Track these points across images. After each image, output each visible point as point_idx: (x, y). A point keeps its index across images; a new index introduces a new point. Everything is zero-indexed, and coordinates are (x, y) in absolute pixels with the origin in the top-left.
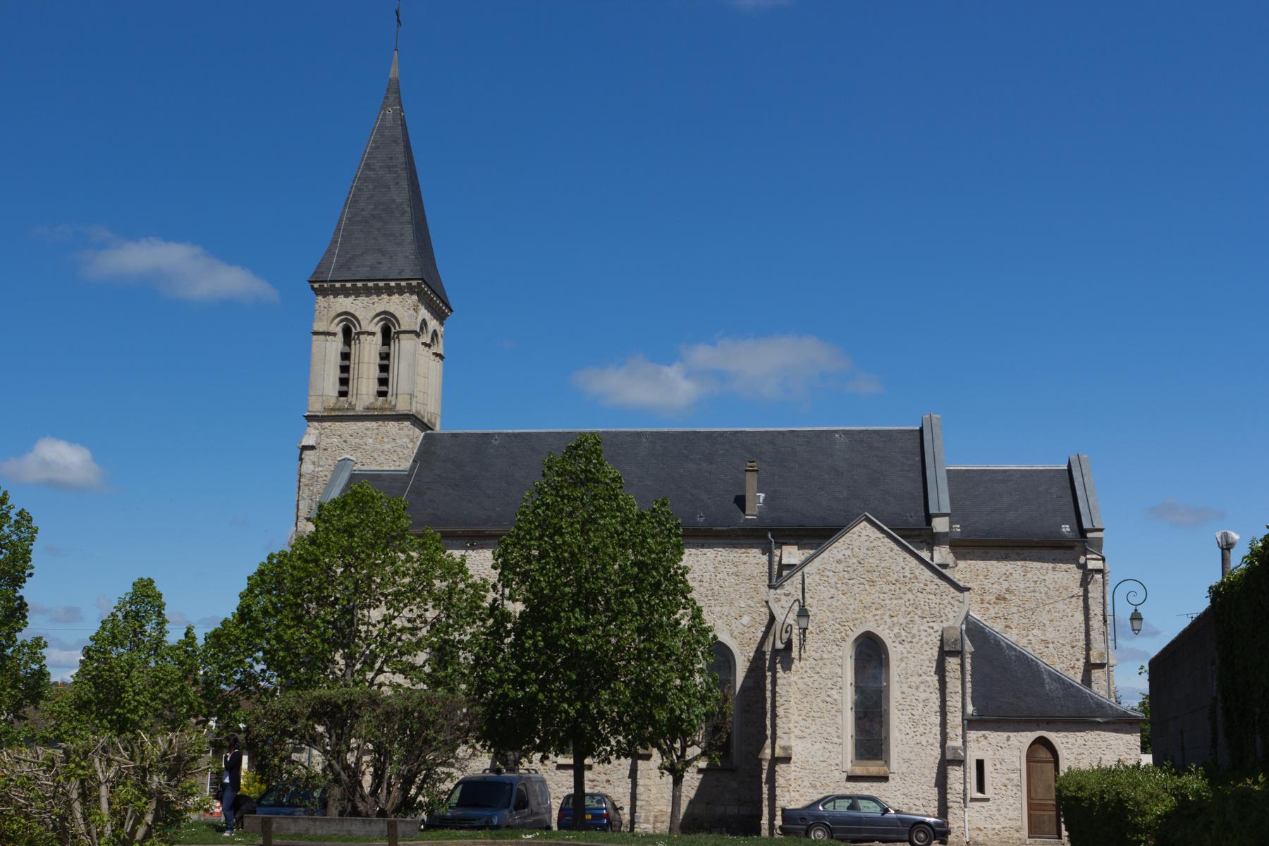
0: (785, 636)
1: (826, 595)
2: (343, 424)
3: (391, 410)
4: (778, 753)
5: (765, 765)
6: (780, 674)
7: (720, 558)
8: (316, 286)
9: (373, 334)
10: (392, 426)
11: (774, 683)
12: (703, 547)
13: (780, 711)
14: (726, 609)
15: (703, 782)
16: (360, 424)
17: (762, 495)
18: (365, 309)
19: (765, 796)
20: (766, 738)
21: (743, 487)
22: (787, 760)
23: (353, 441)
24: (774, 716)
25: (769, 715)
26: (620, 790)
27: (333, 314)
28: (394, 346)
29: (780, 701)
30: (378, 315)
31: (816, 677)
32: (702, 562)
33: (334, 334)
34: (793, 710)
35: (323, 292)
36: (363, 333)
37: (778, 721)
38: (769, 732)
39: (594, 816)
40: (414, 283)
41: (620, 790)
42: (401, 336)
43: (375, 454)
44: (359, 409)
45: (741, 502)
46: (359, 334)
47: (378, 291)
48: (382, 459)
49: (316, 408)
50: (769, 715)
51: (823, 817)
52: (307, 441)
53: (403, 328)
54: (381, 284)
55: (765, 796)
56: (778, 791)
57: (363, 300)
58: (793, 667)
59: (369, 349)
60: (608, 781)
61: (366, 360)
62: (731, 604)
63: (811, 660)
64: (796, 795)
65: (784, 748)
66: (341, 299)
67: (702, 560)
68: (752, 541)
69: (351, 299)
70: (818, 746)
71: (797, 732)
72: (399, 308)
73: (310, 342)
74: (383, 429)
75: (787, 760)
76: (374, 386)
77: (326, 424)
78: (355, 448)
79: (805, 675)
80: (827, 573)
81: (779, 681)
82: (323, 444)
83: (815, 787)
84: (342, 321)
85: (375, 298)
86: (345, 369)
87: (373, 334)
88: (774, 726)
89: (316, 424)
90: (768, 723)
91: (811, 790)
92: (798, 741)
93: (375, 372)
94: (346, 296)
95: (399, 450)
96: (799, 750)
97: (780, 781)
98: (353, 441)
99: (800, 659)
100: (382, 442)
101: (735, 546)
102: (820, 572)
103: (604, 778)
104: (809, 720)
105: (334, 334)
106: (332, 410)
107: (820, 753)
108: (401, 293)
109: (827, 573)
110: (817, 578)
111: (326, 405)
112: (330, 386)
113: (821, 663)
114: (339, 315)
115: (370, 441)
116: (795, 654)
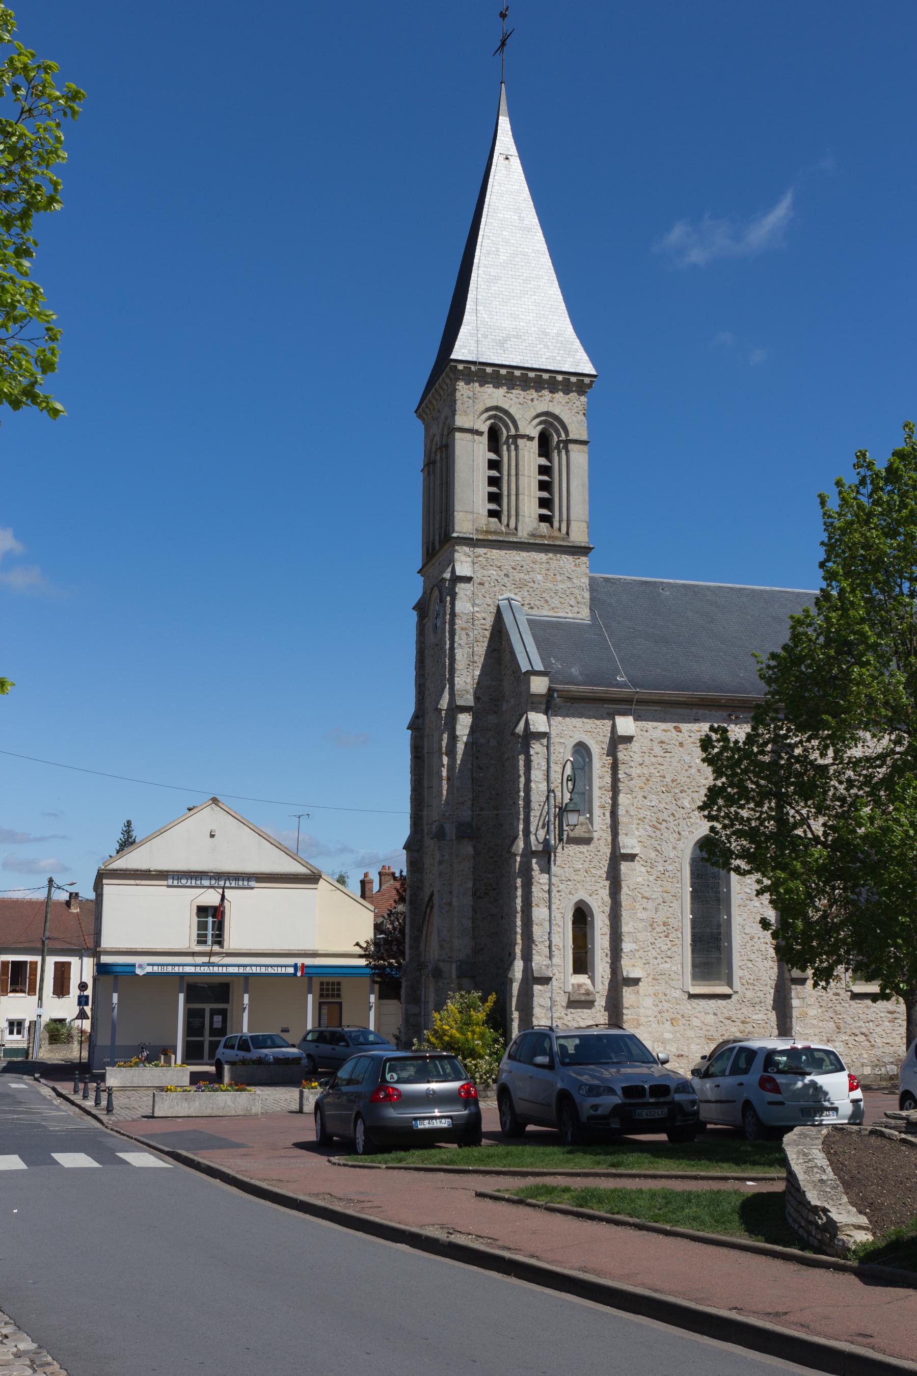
2: (503, 552)
16: (524, 554)
23: (518, 576)
27: (481, 407)
36: (523, 436)
39: (402, 899)
42: (571, 447)
44: (523, 534)
48: (555, 602)
57: (517, 394)
61: (526, 472)
66: (489, 389)
69: (502, 391)
73: (589, 437)
74: (554, 563)
76: (483, 506)
78: (520, 586)
84: (489, 418)
85: (533, 394)
86: (493, 481)
89: (466, 549)
93: (483, 489)
94: (497, 386)
95: (576, 592)
98: (518, 576)
106: (483, 532)
108: (567, 392)
114: (487, 410)
115: (540, 577)
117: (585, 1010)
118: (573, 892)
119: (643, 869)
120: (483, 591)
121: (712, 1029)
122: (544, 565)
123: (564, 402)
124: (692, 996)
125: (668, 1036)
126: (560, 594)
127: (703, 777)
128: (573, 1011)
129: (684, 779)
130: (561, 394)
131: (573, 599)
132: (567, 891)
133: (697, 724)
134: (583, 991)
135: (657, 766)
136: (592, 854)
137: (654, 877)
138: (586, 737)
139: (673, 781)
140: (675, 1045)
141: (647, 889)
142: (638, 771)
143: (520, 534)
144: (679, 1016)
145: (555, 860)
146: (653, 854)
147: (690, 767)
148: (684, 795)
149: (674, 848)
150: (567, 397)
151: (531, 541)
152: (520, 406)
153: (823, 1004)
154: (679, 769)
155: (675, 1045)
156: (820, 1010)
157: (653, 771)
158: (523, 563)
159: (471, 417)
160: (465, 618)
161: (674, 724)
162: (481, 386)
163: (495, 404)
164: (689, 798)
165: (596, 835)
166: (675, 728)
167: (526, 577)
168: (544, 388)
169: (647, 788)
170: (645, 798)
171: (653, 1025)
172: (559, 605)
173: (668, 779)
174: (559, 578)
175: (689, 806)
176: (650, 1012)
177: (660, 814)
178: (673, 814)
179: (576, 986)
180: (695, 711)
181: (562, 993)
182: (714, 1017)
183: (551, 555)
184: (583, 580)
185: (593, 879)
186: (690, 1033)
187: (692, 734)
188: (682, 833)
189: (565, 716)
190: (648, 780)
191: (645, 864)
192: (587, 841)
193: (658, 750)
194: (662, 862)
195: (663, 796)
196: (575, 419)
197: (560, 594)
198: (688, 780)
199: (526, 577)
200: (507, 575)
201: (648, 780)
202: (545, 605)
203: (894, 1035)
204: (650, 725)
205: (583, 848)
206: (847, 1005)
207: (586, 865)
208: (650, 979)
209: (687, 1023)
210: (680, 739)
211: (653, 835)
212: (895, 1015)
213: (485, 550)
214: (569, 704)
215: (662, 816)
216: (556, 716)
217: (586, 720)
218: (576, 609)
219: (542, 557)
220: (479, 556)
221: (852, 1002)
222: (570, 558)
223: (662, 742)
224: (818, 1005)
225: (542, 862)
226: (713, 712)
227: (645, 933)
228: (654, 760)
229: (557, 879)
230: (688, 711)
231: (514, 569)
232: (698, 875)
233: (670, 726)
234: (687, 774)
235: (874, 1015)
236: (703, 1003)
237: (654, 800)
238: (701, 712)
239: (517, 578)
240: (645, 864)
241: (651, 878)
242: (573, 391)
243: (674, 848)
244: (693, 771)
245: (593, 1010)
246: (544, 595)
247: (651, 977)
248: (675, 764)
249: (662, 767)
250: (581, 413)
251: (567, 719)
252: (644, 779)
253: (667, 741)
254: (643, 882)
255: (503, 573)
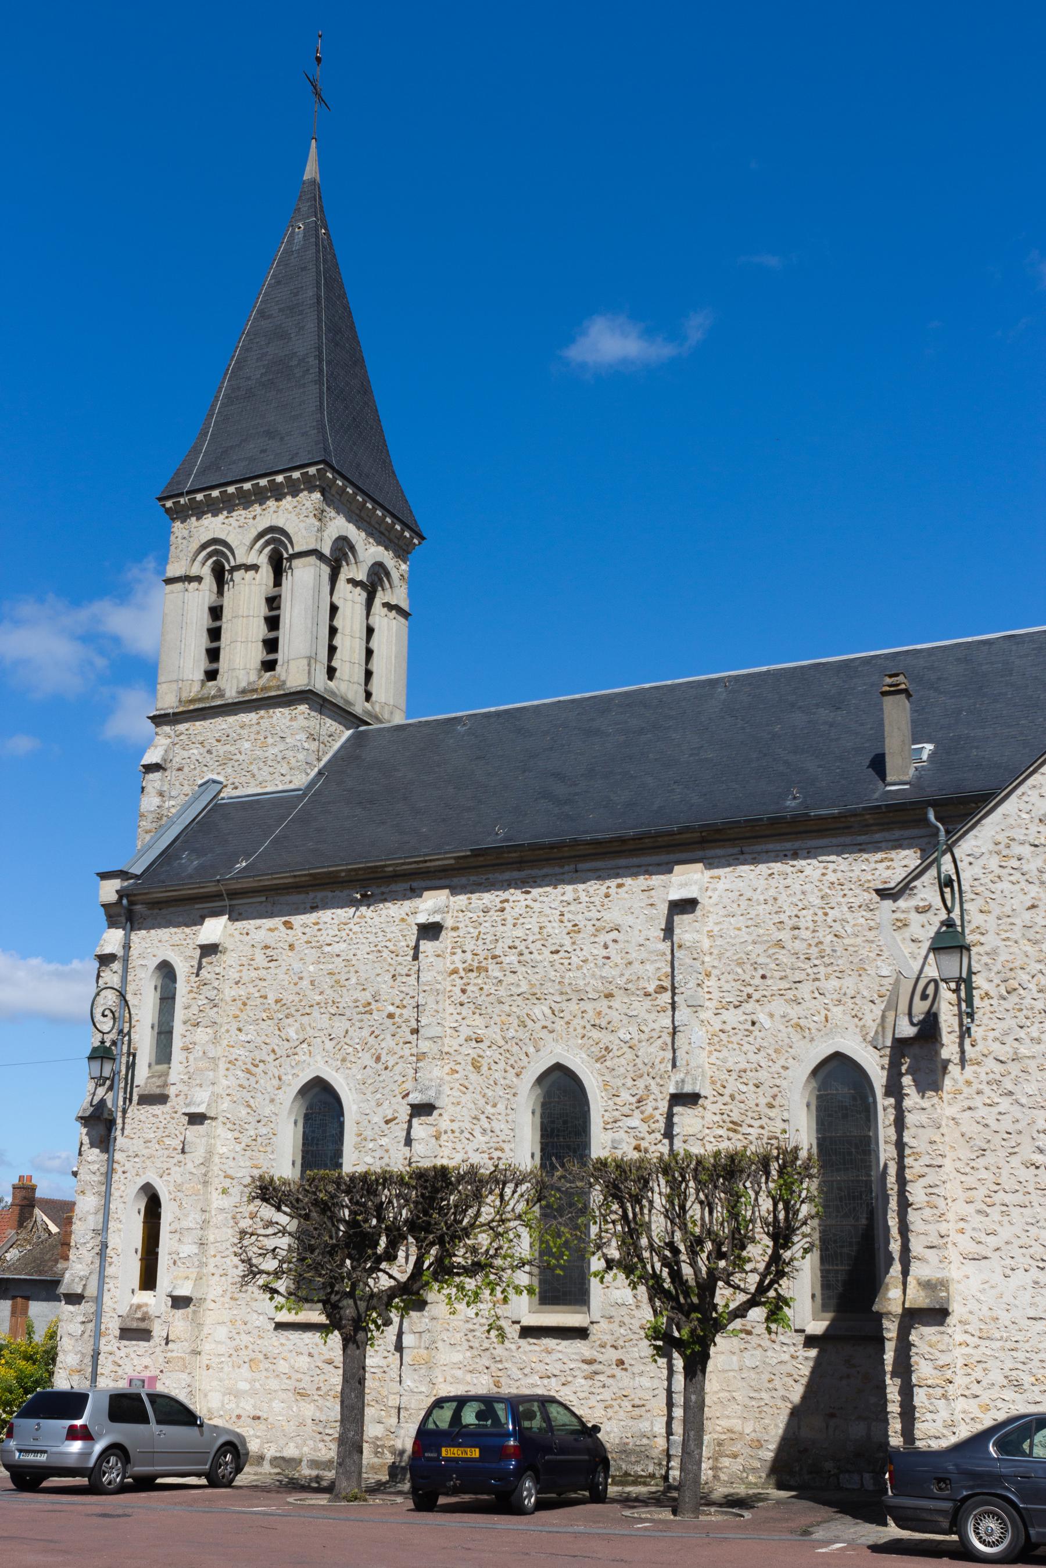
0: (921, 1008)
1: (1019, 902)
3: (278, 688)
4: (917, 1297)
5: (891, 1329)
6: (912, 1099)
7: (832, 877)
8: (169, 504)
9: (255, 567)
10: (280, 716)
11: (900, 1124)
12: (795, 856)
13: (916, 1193)
14: (849, 983)
15: (818, 1369)
16: (231, 719)
17: (929, 747)
18: (238, 529)
19: (894, 1408)
20: (890, 1260)
21: (879, 736)
22: (938, 1315)
23: (221, 749)
24: (904, 1204)
25: (893, 1204)
26: (645, 1382)
27: (195, 546)
28: (287, 581)
29: (914, 1166)
30: (260, 535)
31: (1005, 1104)
32: (796, 887)
33: (199, 579)
34: (953, 1189)
35: (180, 514)
37: (912, 1216)
38: (895, 1247)
40: (312, 470)
41: (645, 1382)
42: (296, 563)
43: (254, 768)
44: (231, 694)
45: (878, 765)
46: (234, 569)
47: (260, 496)
49: (168, 701)
50: (893, 1204)
51: (998, 1479)
52: (152, 757)
53: (297, 549)
54: (263, 482)
55: (894, 1408)
56: (920, 1398)
58: (948, 1082)
59: (247, 595)
60: (620, 1363)
62: (861, 971)
63: (990, 1064)
64: (972, 1406)
65: (928, 1286)
66: (208, 520)
67: (796, 883)
68: (897, 834)
70: (1019, 1278)
71: (965, 1244)
72: (293, 516)
75: (938, 1315)
76: (257, 654)
77: (181, 727)
78: (223, 762)
79: (978, 1101)
80: (1017, 849)
81: (910, 1119)
82: (177, 761)
83: (1018, 1386)
84: (210, 556)
87: (255, 567)
88: (904, 1230)
89: (167, 729)
90: (893, 1222)
91: (1009, 1394)
92: (970, 1267)
95: (289, 754)
96: (969, 1290)
97: (923, 1370)
98: (221, 749)
99: (963, 1062)
100: (264, 746)
101: (862, 848)
102: (1001, 849)
103: (613, 1355)
104: (995, 1213)
105: (199, 579)
106: (192, 701)
107: (1026, 1297)
109: (1017, 849)
110: (994, 862)
111: (185, 696)
112: (195, 665)
113: (1015, 1068)
114: (204, 547)
115: (247, 745)
116: (949, 1050)
117: (141, 1343)
118: (141, 1171)
119: (230, 1135)
120: (181, 778)
121: (308, 1378)
122: (255, 728)
123: (290, 509)
124: (280, 1326)
125: (244, 1386)
126: (269, 763)
127: (317, 991)
128: (127, 1343)
129: (291, 998)
130: (289, 498)
131: (285, 765)
132: (134, 1172)
133: (314, 914)
134: (139, 1315)
135: (258, 982)
136: (168, 1117)
137: (243, 1145)
138: (172, 954)
139: (277, 1002)
140: (252, 1401)
141: (231, 1163)
142: (233, 993)
143: (228, 694)
144: (261, 1357)
145: (123, 1129)
146: (244, 1111)
147: (301, 978)
148: (290, 1020)
149: (272, 1101)
150: (295, 500)
151: (241, 699)
152: (239, 530)
153: (476, 1345)
154: (286, 983)
155: (252, 1401)
156: (468, 1354)
157: (252, 990)
158: (230, 731)
159: (183, 562)
160: (150, 817)
161: (284, 919)
162: (198, 519)
163: (210, 536)
164: (297, 1025)
165: (172, 1091)
166: (285, 923)
167: (232, 749)
168: (268, 498)
169: (243, 1016)
170: (240, 1030)
171: (226, 1369)
172: (269, 778)
173: (271, 1000)
174: (270, 741)
175: (295, 1037)
176: (222, 1349)
177: (257, 1052)
178: (273, 1051)
179: (134, 1308)
180: (311, 895)
181: (116, 1316)
182: (308, 1359)
183: (262, 712)
184: (298, 737)
185: (166, 1152)
186: (273, 1384)
187: (307, 930)
188: (284, 1078)
189: (148, 928)
190: (245, 1004)
191: (232, 1127)
192: (161, 1099)
193: (260, 959)
194: (254, 1123)
195: (263, 1025)
196: (302, 525)
197: (269, 763)
198: (297, 999)
199: (232, 749)
200: (209, 752)
201: (245, 1004)
202: (252, 780)
203: (593, 1402)
204: (250, 924)
205: (157, 1109)
206: (513, 1347)
207: (159, 1133)
208: (227, 1299)
209: (272, 1367)
210: (290, 939)
211: (246, 1083)
212: (595, 1367)
213: (186, 725)
214: (156, 911)
215: (258, 1055)
216: (139, 929)
217: (173, 930)
218: (288, 778)
219: (249, 718)
220: (181, 734)
221: (523, 1342)
222: (286, 711)
223: (266, 947)
224: (466, 1345)
225: (94, 1133)
226: (338, 893)
227: (224, 1229)
228: (254, 974)
229: (124, 1155)
230: (302, 896)
231: (218, 741)
232: (552, 1130)
233: (277, 922)
234: (296, 989)
235: (559, 1366)
236: (294, 1336)
237: (250, 1033)
238: (320, 895)
239: (221, 753)
240: (232, 1127)
241: (238, 1148)
242: (302, 491)
243: (272, 1101)
244: (305, 983)
245: (152, 1343)
246: (251, 767)
247: (229, 1295)
248: (281, 976)
249: (264, 984)
250: (311, 515)
251: (152, 931)
252: (239, 1003)
253: (273, 945)
254: (228, 1154)
255: (206, 750)
